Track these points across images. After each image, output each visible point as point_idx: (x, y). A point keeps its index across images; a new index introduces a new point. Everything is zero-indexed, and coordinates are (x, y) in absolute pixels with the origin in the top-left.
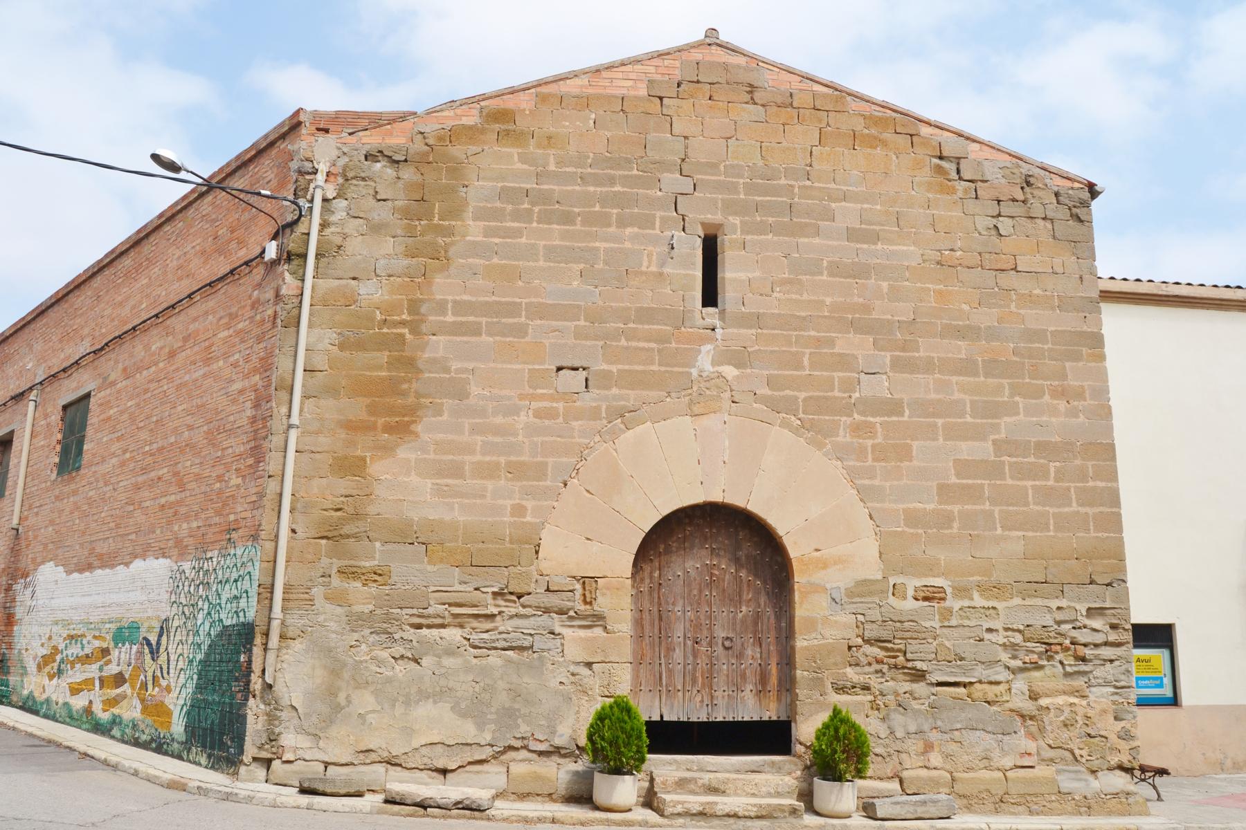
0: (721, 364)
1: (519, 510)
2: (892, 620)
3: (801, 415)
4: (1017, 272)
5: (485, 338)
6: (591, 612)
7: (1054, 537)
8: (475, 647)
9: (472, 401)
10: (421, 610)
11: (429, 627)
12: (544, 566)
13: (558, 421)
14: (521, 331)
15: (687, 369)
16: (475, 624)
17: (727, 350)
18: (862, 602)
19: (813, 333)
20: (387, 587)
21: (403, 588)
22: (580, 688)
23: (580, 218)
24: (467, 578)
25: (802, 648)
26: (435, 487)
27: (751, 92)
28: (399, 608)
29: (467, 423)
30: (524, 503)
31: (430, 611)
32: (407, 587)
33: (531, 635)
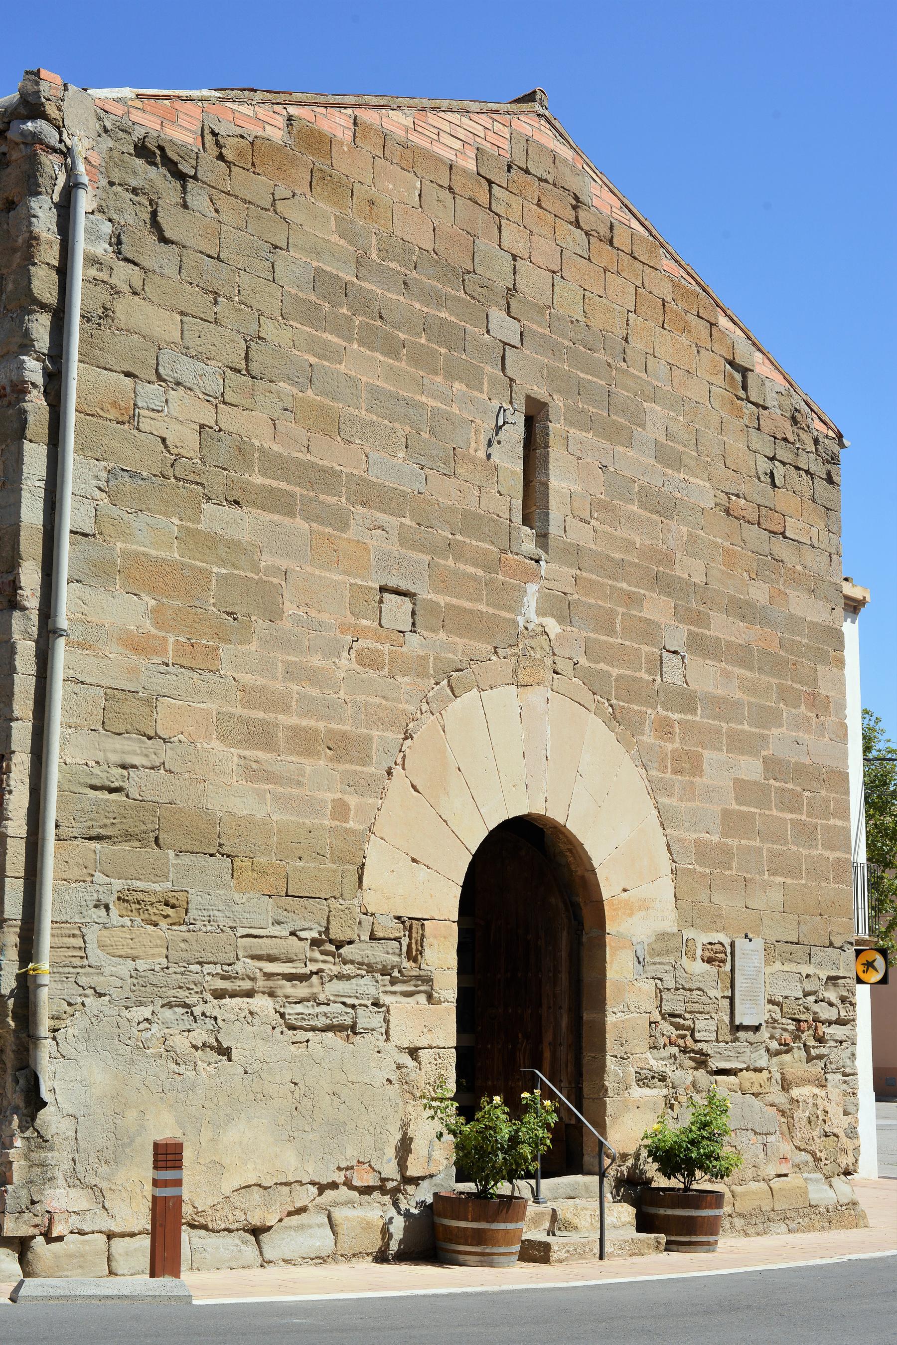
0: (544, 615)
1: (341, 810)
2: (683, 988)
3: (614, 701)
4: (785, 537)
5: (300, 524)
6: (415, 973)
7: (805, 886)
8: (292, 1028)
9: (286, 624)
10: (226, 968)
11: (233, 995)
12: (371, 900)
13: (382, 673)
14: (340, 521)
15: (513, 616)
16: (288, 988)
17: (550, 594)
18: (660, 963)
19: (624, 585)
20: (184, 928)
21: (203, 928)
22: (406, 1087)
23: (405, 351)
24: (282, 916)
25: (615, 1024)
26: (242, 762)
27: (575, 208)
28: (197, 963)
29: (281, 657)
30: (346, 798)
31: (239, 967)
32: (209, 928)
33: (353, 1007)
